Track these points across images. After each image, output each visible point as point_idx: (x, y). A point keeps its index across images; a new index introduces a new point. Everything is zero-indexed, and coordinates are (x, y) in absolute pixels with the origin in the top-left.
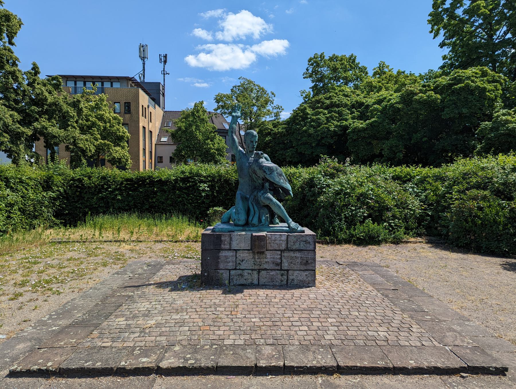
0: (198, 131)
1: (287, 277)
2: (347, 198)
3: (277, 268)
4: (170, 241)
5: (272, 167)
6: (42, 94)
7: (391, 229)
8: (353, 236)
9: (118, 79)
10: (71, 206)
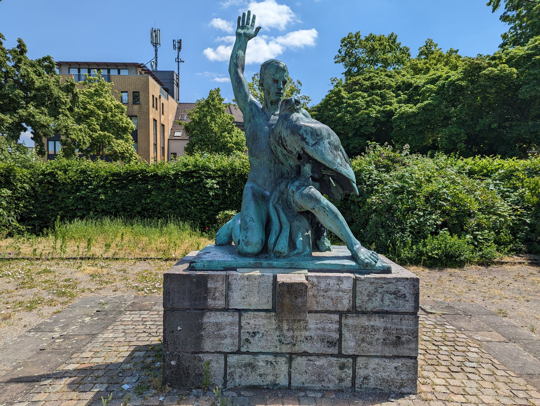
0: (213, 123)
1: (354, 372)
2: (411, 198)
3: (331, 351)
4: (158, 259)
5: (319, 129)
6: (28, 75)
7: (476, 243)
8: (421, 254)
9: (126, 66)
10: (41, 208)
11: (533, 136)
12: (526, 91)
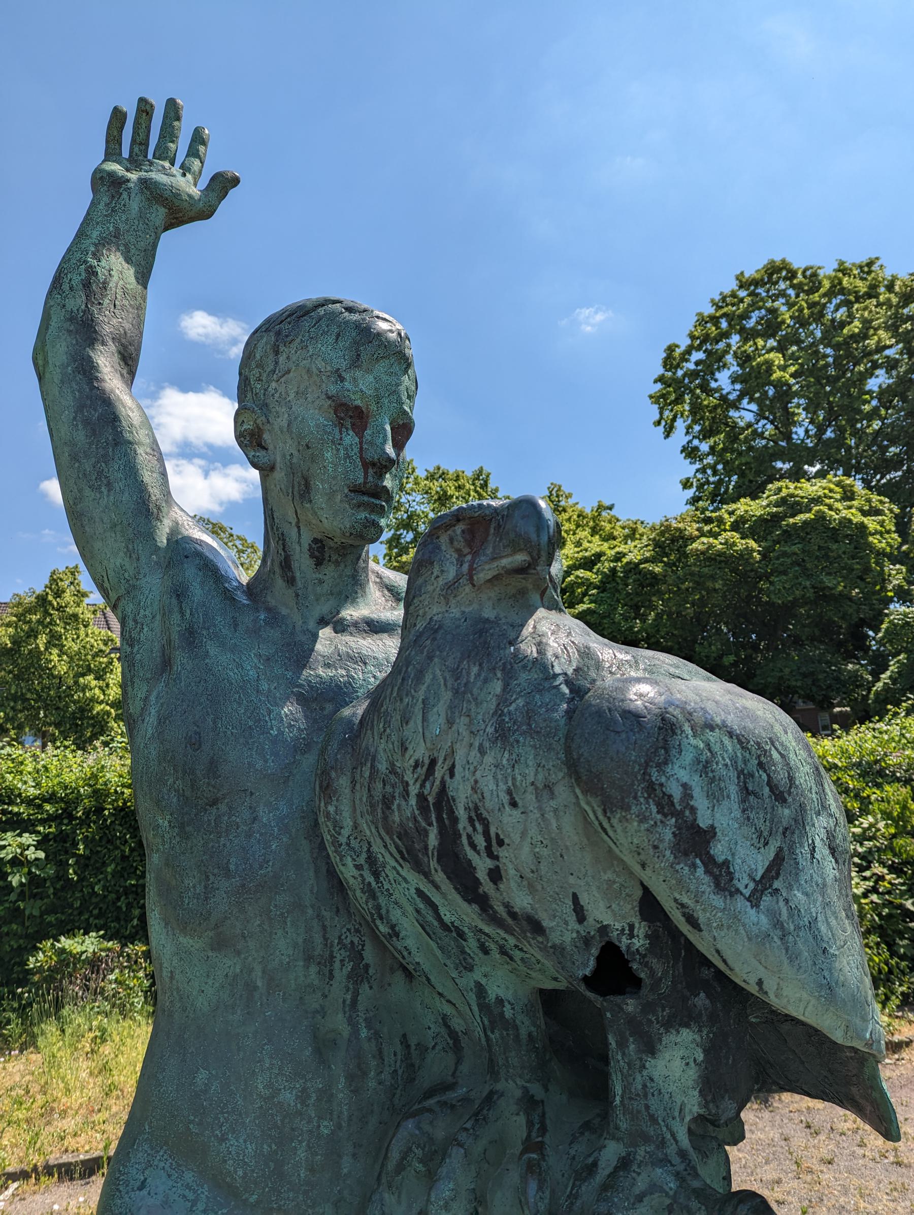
0: (55, 651)
11: (810, 682)
12: (784, 588)
